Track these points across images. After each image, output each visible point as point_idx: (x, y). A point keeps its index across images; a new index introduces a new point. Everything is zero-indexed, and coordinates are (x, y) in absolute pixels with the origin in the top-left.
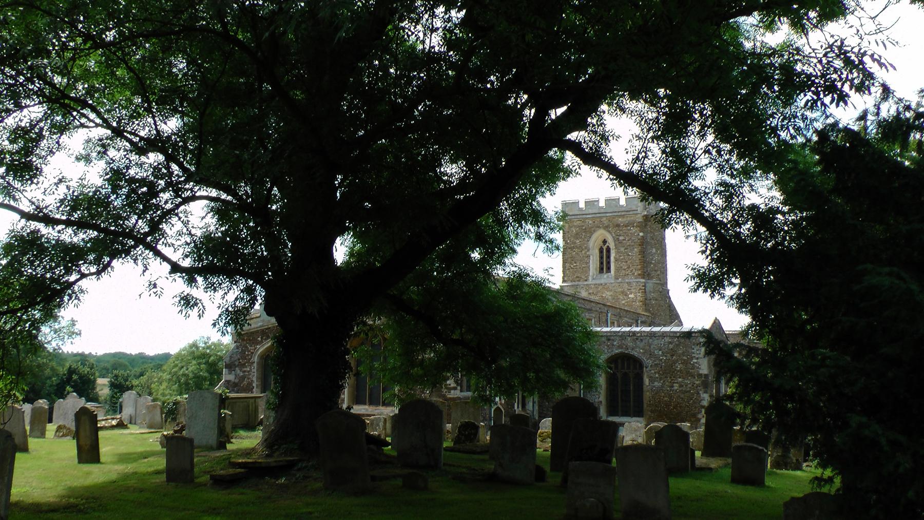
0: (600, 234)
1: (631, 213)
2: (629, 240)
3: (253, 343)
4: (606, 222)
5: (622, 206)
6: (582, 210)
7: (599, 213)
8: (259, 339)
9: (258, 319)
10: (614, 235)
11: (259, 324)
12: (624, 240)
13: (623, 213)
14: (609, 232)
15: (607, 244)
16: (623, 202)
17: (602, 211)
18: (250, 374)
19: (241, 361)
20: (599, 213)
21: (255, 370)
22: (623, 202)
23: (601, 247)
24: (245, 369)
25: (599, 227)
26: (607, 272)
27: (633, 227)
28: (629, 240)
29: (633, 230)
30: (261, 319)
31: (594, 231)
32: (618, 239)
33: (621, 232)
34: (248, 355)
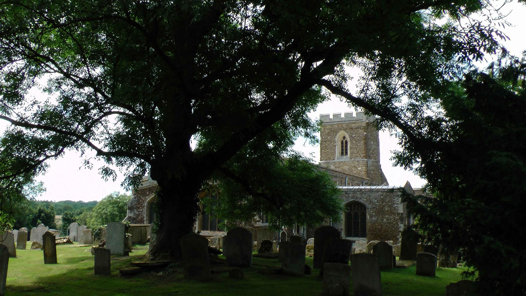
1: (359, 121)
2: (358, 137)
3: (144, 195)
4: (345, 127)
5: (354, 117)
8: (148, 193)
10: (349, 134)
11: (148, 184)
12: (355, 137)
13: (355, 121)
14: (347, 132)
15: (346, 139)
16: (354, 115)
17: (343, 120)
18: (142, 213)
19: (137, 205)
22: (354, 115)
24: (140, 210)
26: (345, 155)
27: (360, 129)
28: (358, 137)
29: (360, 131)
31: (338, 132)
32: (352, 136)
33: (354, 132)
34: (141, 202)
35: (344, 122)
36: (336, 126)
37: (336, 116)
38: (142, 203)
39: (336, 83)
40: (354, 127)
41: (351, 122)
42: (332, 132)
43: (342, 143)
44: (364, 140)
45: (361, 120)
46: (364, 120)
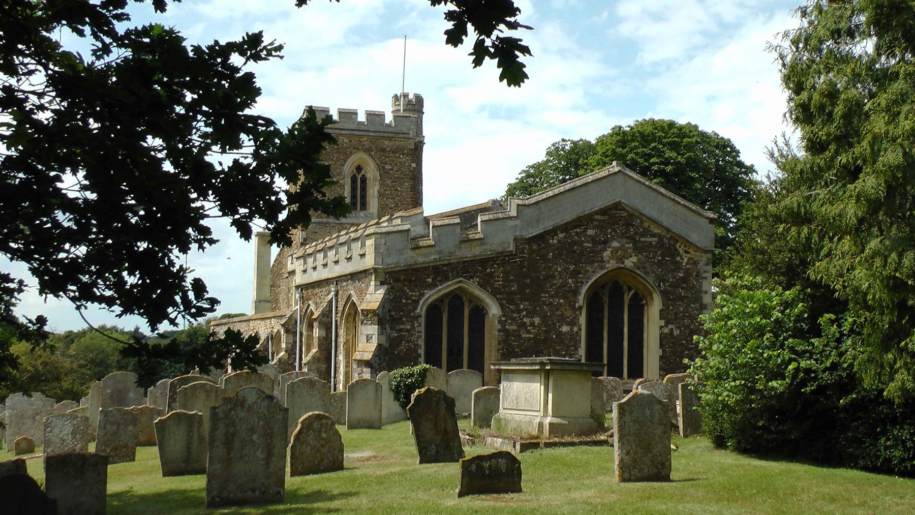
0: (358, 157)
1: (401, 136)
2: (397, 171)
3: (416, 286)
4: (367, 144)
5: (362, 123)
6: (364, 125)
7: (358, 130)
8: (430, 280)
9: (428, 250)
12: (390, 169)
13: (390, 135)
14: (372, 156)
15: (363, 172)
16: (389, 119)
17: (362, 128)
19: (393, 313)
20: (358, 130)
21: (422, 329)
22: (389, 119)
23: (354, 175)
25: (358, 149)
27: (403, 154)
28: (397, 171)
29: (403, 159)
30: (437, 249)
31: (351, 154)
32: (383, 167)
33: (387, 159)
34: (406, 304)
35: (365, 133)
36: (346, 140)
37: (345, 114)
38: (410, 308)
39: (814, 65)
40: (388, 147)
41: (382, 134)
42: (336, 153)
43: (354, 180)
44: (411, 179)
45: (404, 133)
46: (411, 136)
